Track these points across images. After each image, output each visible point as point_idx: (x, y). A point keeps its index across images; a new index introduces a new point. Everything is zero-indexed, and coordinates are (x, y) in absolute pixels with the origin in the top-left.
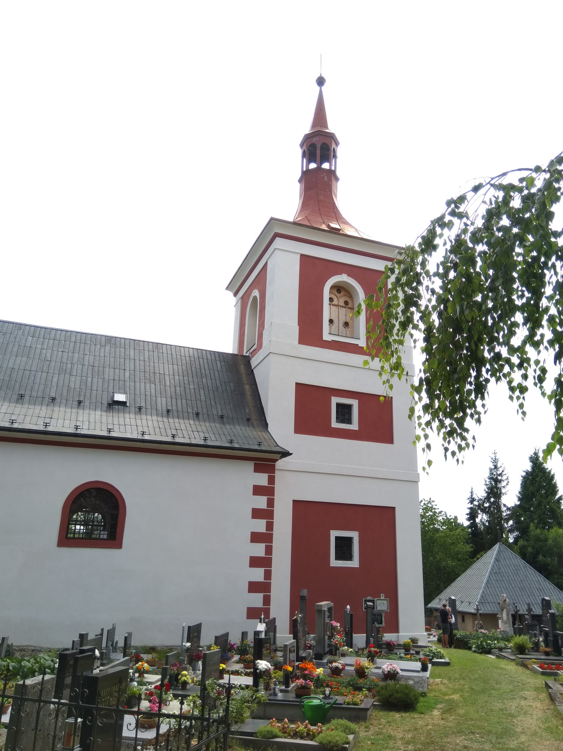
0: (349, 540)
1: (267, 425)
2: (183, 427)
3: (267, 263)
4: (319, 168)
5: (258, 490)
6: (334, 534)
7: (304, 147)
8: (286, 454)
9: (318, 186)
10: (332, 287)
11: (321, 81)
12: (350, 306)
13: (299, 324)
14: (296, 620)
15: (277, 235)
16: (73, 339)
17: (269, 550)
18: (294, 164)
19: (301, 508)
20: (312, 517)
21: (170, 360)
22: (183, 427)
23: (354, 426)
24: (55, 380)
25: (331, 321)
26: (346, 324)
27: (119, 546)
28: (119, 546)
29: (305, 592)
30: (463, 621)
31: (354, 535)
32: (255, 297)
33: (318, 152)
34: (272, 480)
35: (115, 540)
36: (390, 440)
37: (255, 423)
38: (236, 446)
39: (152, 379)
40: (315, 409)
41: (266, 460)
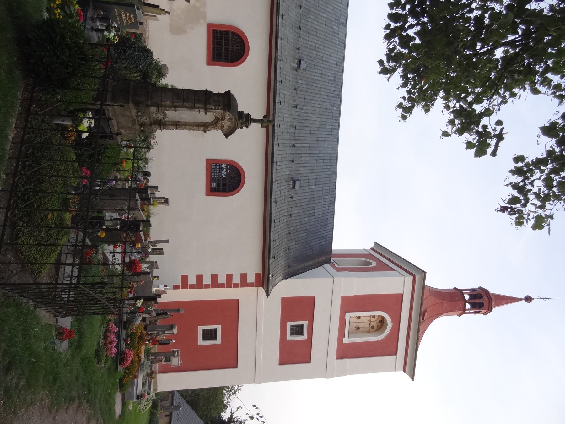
0: (215, 338)
1: (286, 279)
2: (281, 226)
3: (395, 270)
4: (466, 302)
5: (244, 277)
6: (218, 327)
7: (479, 290)
8: (268, 294)
9: (455, 301)
10: (383, 317)
11: (528, 299)
12: (371, 330)
13: (355, 296)
14: (166, 314)
15: (414, 276)
16: (333, 152)
17: (207, 286)
18: (467, 282)
19: (235, 304)
20: (228, 312)
21: (324, 212)
22: (281, 226)
23: (289, 338)
24: (306, 145)
25: (359, 318)
26: (358, 328)
27: (207, 195)
28: (207, 195)
29: (182, 311)
30: (166, 416)
31: (218, 341)
32: (371, 264)
33: (477, 301)
34: (251, 285)
35: (208, 64)
36: (281, 363)
37: (287, 271)
38: (271, 261)
39: (311, 202)
40: (299, 311)
41: (264, 280)
